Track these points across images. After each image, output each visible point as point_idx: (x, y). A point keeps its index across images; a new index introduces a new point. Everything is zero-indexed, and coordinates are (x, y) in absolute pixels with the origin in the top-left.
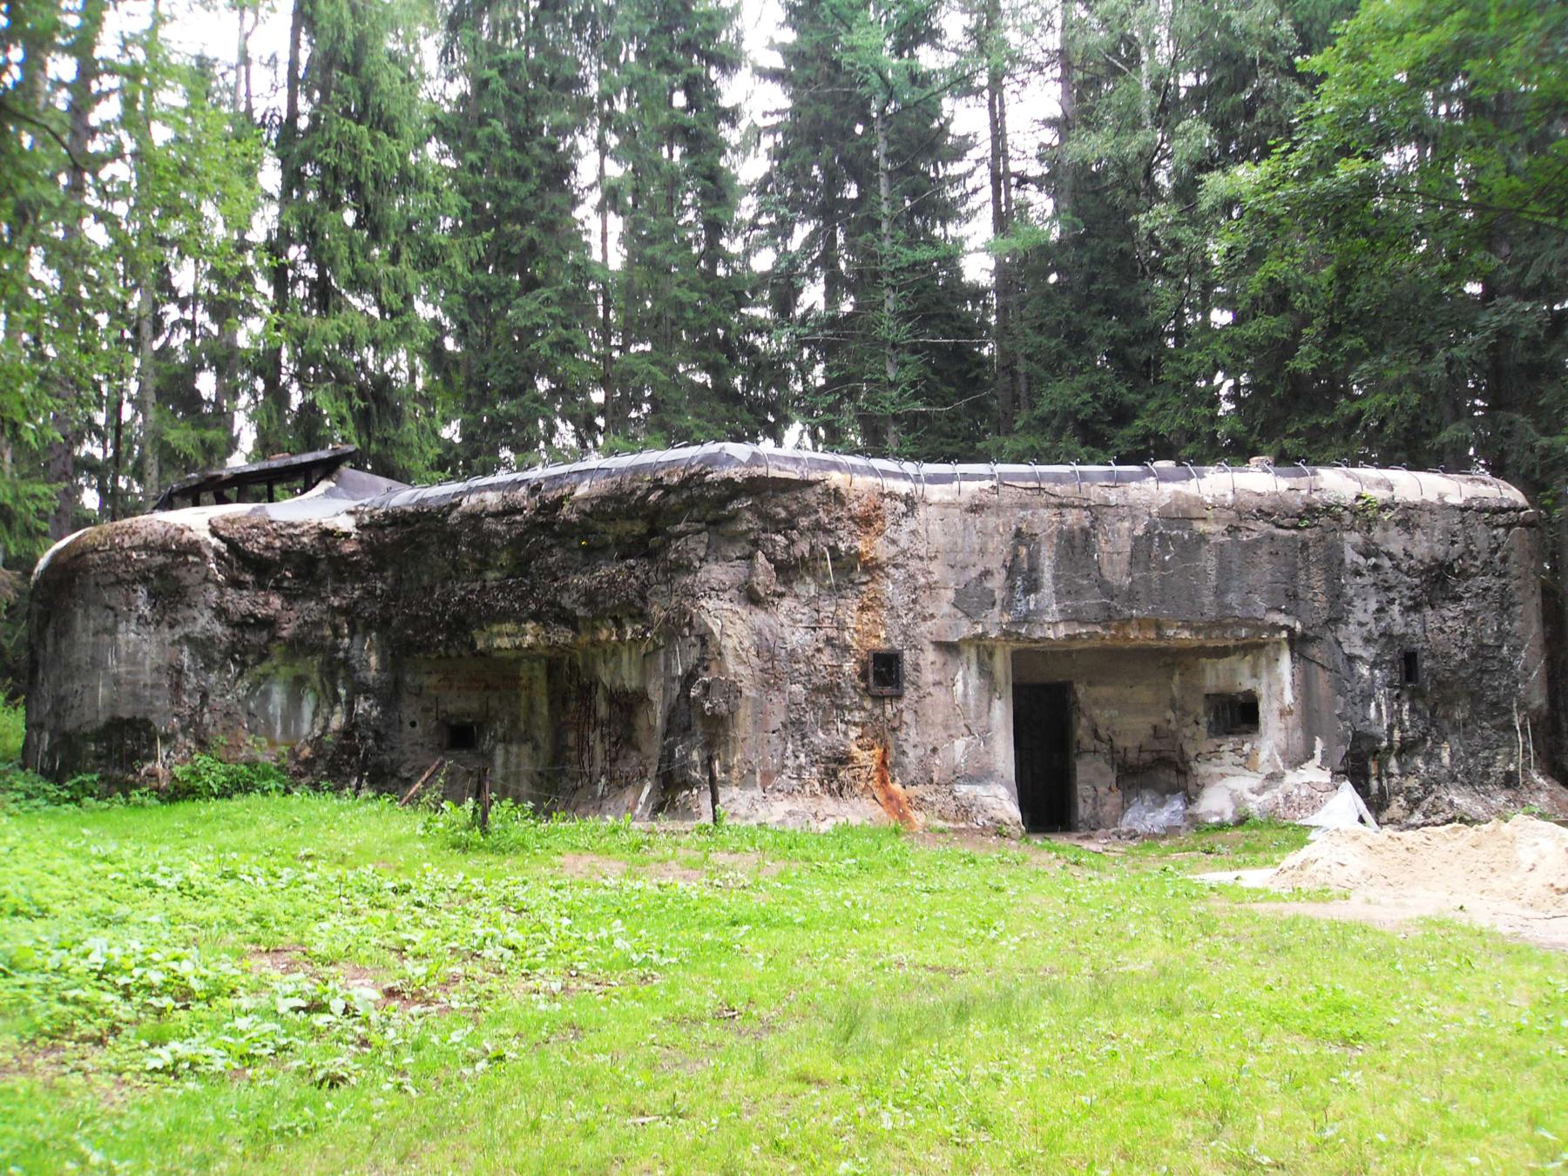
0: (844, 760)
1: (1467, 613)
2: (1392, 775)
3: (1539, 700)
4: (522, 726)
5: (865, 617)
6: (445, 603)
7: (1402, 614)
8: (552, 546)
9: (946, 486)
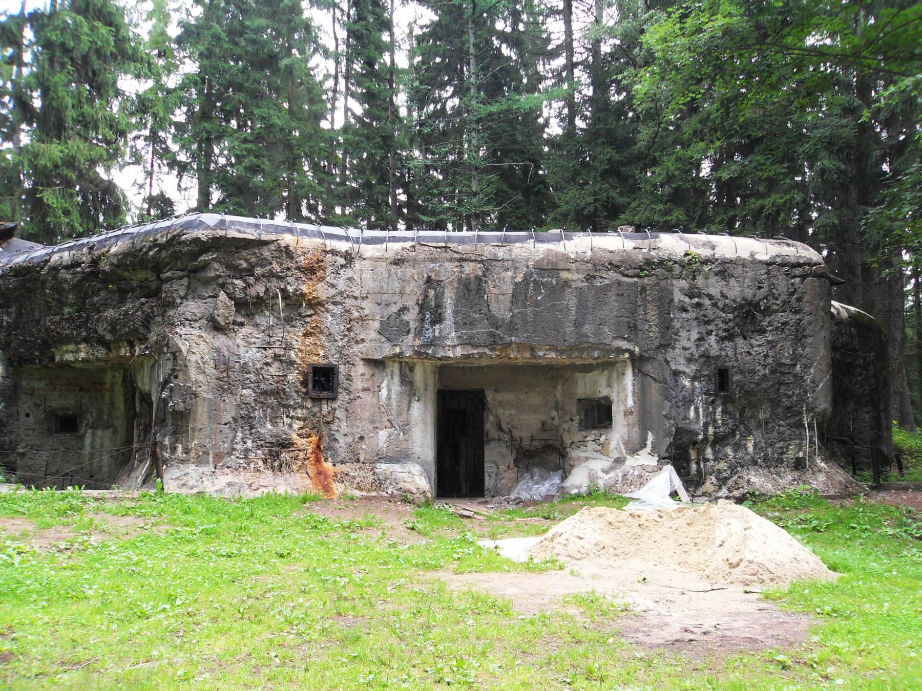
0: (286, 444)
1: (769, 342)
2: (708, 460)
3: (823, 404)
4: (105, 417)
5: (308, 341)
7: (718, 342)
9: (378, 246)
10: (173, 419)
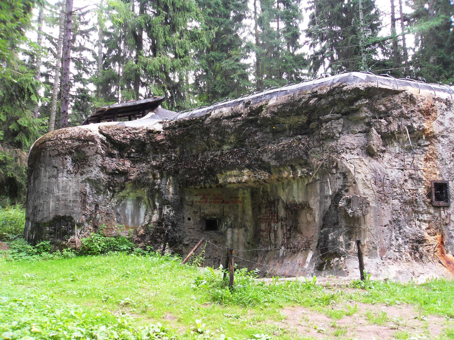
0: (421, 241)
5: (428, 165)
6: (203, 162)
8: (256, 131)
10: (346, 222)
